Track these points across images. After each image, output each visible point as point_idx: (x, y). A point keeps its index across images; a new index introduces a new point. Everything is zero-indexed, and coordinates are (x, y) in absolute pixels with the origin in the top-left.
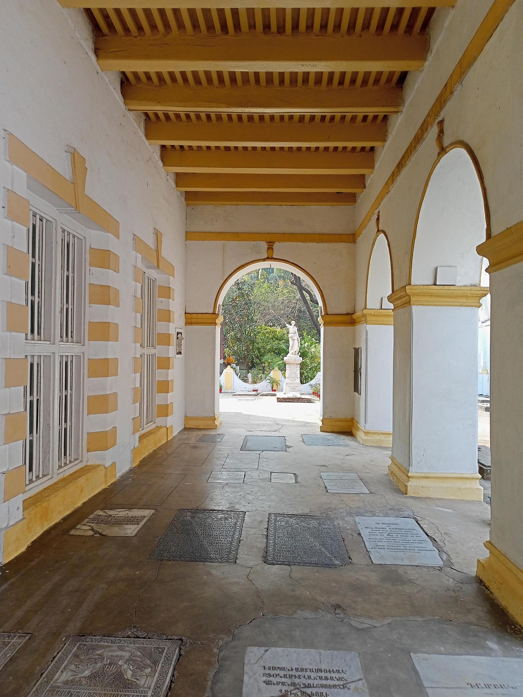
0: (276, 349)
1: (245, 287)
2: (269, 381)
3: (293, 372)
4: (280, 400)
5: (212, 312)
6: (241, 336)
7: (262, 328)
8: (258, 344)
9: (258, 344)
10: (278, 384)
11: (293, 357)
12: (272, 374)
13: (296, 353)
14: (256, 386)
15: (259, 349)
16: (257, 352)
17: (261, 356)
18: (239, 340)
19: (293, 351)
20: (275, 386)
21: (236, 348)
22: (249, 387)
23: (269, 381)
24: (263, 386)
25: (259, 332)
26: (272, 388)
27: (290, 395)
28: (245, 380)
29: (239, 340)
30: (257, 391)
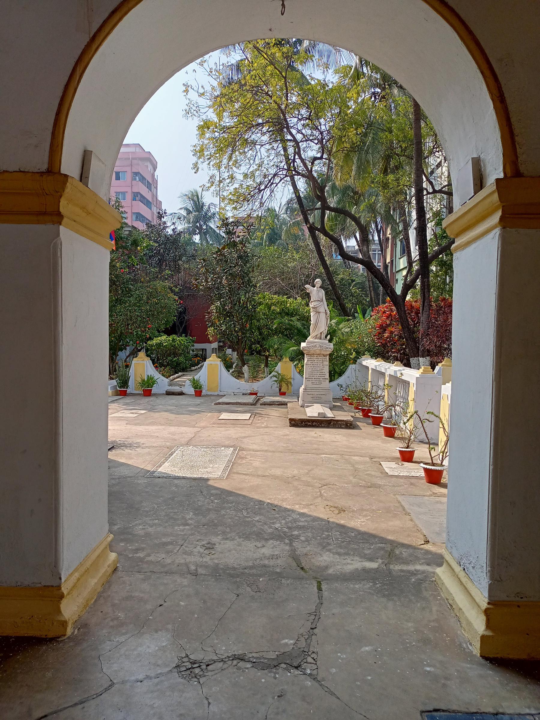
0: (286, 329)
1: (240, 230)
2: (275, 379)
3: (316, 367)
4: (296, 423)
5: (44, 167)
6: (231, 308)
7: (268, 298)
8: (258, 321)
9: (258, 321)
10: (288, 383)
11: (316, 342)
12: (279, 367)
13: (323, 336)
14: (255, 386)
15: (259, 329)
16: (257, 333)
17: (263, 339)
18: (229, 314)
19: (317, 333)
20: (284, 387)
21: (224, 328)
22: (243, 385)
23: (275, 379)
24: (266, 384)
25: (260, 304)
26: (280, 390)
27: (313, 411)
28: (239, 375)
29: (229, 314)
30: (256, 394)
